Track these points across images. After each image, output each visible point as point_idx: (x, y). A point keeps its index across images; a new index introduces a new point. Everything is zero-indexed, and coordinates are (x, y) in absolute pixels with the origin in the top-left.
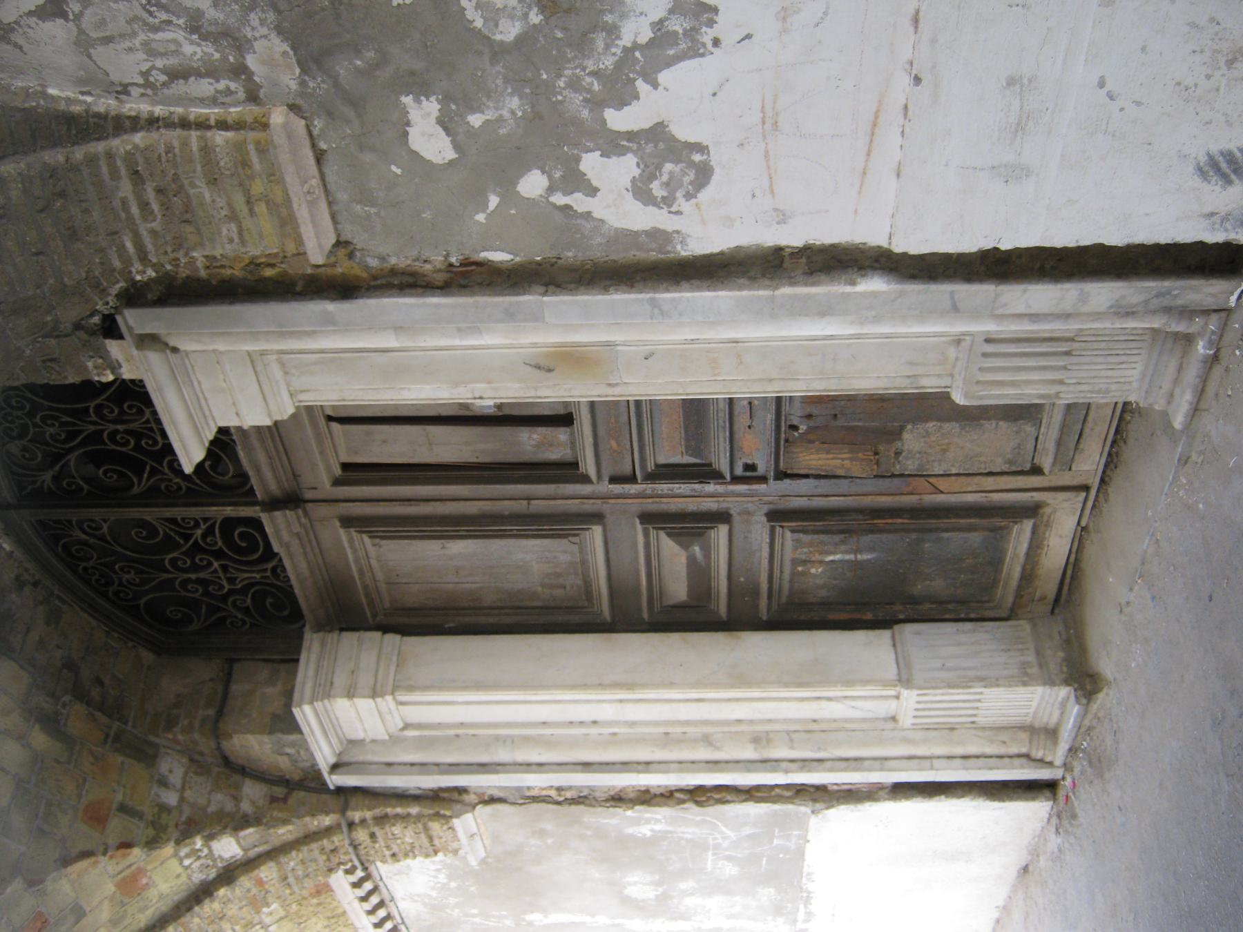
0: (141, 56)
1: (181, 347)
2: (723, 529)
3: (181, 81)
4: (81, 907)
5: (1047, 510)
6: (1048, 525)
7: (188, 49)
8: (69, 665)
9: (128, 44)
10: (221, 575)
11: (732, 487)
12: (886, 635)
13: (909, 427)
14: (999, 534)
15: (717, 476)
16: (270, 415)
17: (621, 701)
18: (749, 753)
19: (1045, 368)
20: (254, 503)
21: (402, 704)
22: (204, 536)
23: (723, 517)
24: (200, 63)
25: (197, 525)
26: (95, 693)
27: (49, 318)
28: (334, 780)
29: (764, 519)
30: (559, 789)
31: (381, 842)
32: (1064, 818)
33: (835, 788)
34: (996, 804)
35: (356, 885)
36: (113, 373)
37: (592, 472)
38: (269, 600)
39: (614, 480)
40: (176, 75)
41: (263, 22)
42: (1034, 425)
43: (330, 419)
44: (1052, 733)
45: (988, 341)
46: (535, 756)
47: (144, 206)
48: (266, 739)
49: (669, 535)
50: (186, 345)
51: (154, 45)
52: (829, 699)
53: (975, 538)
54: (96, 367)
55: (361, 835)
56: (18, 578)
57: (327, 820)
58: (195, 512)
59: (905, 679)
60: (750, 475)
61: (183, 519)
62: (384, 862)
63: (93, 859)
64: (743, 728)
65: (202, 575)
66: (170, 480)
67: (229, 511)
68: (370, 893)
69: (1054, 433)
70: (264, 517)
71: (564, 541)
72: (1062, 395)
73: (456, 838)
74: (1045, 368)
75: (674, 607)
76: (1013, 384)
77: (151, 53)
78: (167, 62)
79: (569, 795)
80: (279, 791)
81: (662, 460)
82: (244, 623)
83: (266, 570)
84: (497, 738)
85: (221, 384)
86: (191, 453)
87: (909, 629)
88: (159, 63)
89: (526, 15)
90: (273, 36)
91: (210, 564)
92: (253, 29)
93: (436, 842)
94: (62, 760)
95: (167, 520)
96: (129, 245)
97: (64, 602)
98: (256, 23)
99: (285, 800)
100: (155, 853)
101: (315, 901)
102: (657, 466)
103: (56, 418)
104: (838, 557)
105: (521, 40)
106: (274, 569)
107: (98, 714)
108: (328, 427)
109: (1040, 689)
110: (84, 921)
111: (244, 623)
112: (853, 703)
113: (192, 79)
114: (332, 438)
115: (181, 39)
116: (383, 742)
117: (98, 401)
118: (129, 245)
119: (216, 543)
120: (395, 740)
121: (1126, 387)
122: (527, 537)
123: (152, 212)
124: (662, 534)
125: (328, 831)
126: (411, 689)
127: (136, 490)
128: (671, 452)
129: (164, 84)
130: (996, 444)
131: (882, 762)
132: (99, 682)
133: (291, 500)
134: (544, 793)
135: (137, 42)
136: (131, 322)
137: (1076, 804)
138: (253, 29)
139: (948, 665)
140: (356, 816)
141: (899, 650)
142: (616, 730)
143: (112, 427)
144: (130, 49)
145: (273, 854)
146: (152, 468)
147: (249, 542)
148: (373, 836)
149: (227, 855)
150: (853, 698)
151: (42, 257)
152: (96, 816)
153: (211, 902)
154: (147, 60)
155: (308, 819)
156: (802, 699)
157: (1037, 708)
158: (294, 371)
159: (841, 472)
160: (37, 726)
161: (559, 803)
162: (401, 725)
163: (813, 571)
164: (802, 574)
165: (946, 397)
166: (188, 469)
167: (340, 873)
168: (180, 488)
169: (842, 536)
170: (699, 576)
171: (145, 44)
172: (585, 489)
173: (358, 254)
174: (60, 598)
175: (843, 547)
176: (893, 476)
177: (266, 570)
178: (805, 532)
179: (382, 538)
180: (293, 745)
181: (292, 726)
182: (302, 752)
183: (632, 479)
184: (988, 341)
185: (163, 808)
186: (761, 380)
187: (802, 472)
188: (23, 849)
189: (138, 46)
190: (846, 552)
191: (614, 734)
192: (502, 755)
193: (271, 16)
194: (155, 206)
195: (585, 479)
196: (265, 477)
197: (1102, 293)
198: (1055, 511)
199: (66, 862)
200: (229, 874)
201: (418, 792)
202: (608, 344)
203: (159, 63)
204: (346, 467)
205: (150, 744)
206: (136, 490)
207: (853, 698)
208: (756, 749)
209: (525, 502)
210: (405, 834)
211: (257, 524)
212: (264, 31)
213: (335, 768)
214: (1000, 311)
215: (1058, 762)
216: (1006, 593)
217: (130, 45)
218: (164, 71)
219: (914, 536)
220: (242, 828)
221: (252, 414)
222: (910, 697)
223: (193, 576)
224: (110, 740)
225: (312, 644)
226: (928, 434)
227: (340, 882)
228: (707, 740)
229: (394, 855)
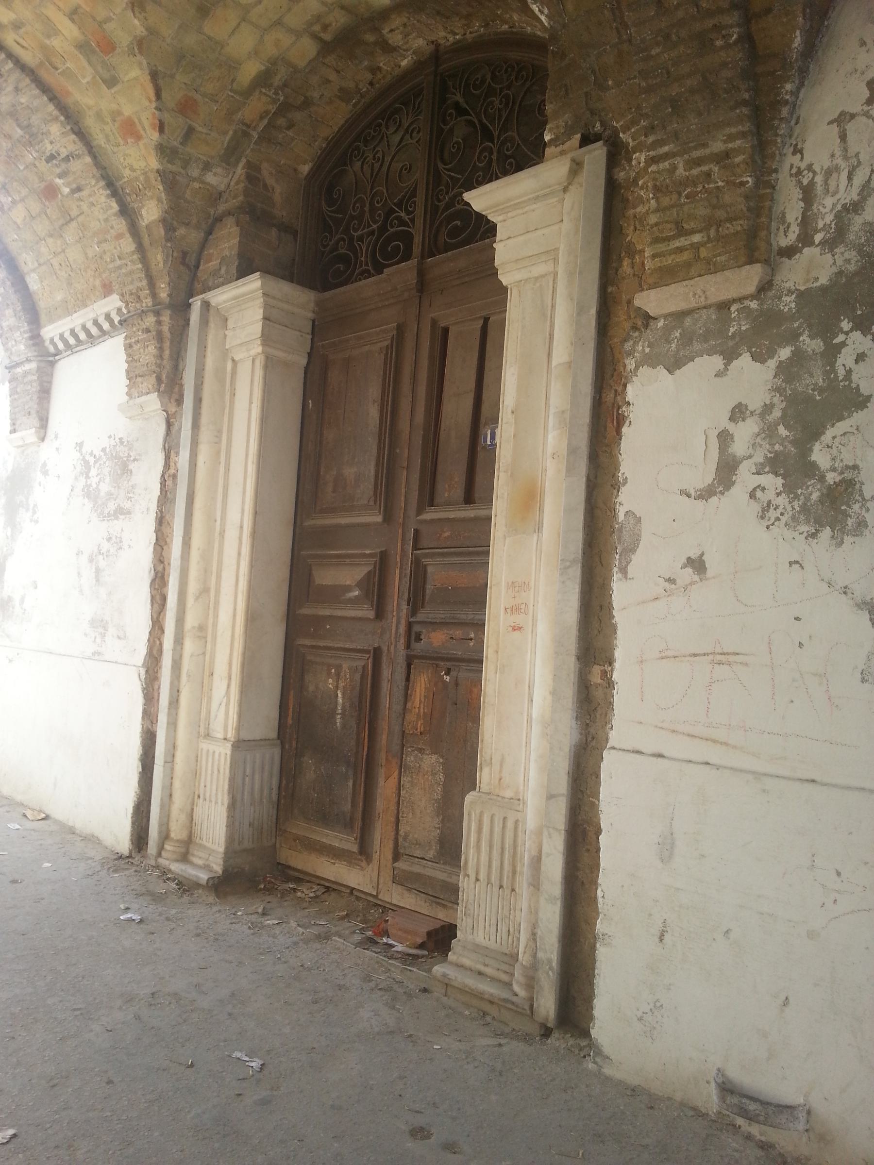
0: (827, 164)
1: (567, 196)
2: (371, 614)
3: (801, 196)
4: (115, 85)
5: (364, 864)
6: (350, 863)
7: (829, 201)
8: (307, 103)
9: (838, 153)
10: (366, 230)
11: (403, 622)
12: (274, 735)
13: (441, 760)
14: (348, 825)
15: (414, 612)
16: (503, 264)
17: (241, 527)
18: (191, 621)
19: (490, 866)
20: (423, 257)
21: (254, 360)
22: (399, 218)
23: (380, 614)
24: (815, 211)
25: (408, 213)
26: (281, 121)
27: (610, 83)
28: (196, 303)
29: (376, 645)
30: (174, 477)
31: (142, 336)
32: (118, 861)
33: (156, 687)
34: (130, 811)
35: (108, 317)
36: (551, 141)
37: (427, 516)
38: (342, 267)
39: (416, 532)
40: (808, 194)
41: (848, 261)
42: (434, 857)
43: (486, 320)
44: (184, 858)
45: (517, 822)
46: (201, 459)
47: (698, 162)
48: (235, 252)
49: (369, 572)
50: (569, 199)
51: (835, 175)
52: (229, 686)
53: (347, 807)
54: (558, 127)
55: (150, 320)
56: (379, 69)
57: (163, 295)
58: (419, 212)
59: (239, 745)
60: (412, 636)
61: (415, 202)
62: (126, 338)
63: (154, 99)
64: (211, 620)
65: (367, 215)
66: (447, 193)
67: (417, 240)
68: (100, 327)
69: (429, 872)
70: (413, 262)
71: (372, 493)
72: (466, 878)
73: (141, 394)
74: (490, 866)
75: (310, 574)
76: (479, 840)
77: (828, 173)
78: (819, 185)
79: (169, 483)
80: (192, 260)
81: (430, 569)
82: (325, 246)
83: (367, 265)
84: (220, 431)
85: (536, 223)
86: (480, 199)
87: (277, 752)
88: (819, 179)
89: (833, 469)
90: (835, 269)
91: (375, 222)
92: (842, 253)
93: (139, 379)
94: (234, 85)
95: (415, 189)
96: (666, 149)
97: (355, 105)
98: (847, 255)
99: (183, 263)
100: (153, 153)
101: (98, 283)
102: (426, 565)
103: (507, 104)
104: (340, 700)
105: (814, 465)
106: (368, 271)
107: (265, 121)
108: (481, 317)
109: (221, 849)
110: (104, 87)
111: (325, 246)
112: (224, 704)
113: (802, 204)
114: (470, 320)
115: (837, 197)
116: (224, 344)
117: (517, 138)
118: (666, 149)
119: (392, 227)
120: (225, 353)
121: (469, 930)
122: (377, 465)
123: (691, 169)
124: (371, 568)
125: (154, 295)
126: (266, 367)
127: (441, 166)
128: (438, 574)
129: (800, 182)
130: (421, 823)
131: (173, 724)
132: (290, 126)
133: (422, 286)
134: (172, 464)
135: (839, 161)
136: (597, 153)
137: (127, 872)
138: (842, 253)
139: (247, 779)
140: (166, 318)
141: (262, 743)
142: (218, 522)
143: (495, 150)
144: (833, 156)
145: (140, 248)
146: (459, 179)
147: (391, 249)
148: (148, 331)
149: (144, 212)
150: (228, 704)
151: (666, 76)
152: (186, 107)
153: (108, 196)
154: (822, 169)
155: (167, 279)
156: (230, 664)
157: (205, 847)
158: (538, 285)
159: (409, 705)
160: (263, 68)
161: (163, 476)
162: (236, 358)
163: (330, 681)
164: (329, 674)
165: (473, 787)
166: (468, 196)
167: (120, 304)
168: (440, 201)
169: (357, 704)
170: (334, 594)
171: (837, 169)
172: (412, 512)
173: (637, 334)
174: (359, 102)
175: (348, 704)
176: (403, 746)
177: (367, 265)
178: (363, 677)
179: (386, 355)
180: (227, 272)
181: (243, 272)
182: (221, 280)
183: (415, 548)
184: (517, 822)
185: (186, 164)
186: (498, 644)
187: (412, 676)
188: (169, 40)
189: (834, 162)
190: (343, 707)
191: (216, 521)
192: (205, 435)
193: (852, 268)
194: (695, 172)
195: (419, 512)
196: (445, 264)
197: (551, 916)
198: (362, 869)
199: (154, 76)
200: (126, 212)
201: (181, 367)
202: (539, 528)
203: (819, 179)
204: (446, 331)
205: (238, 161)
206: (441, 166)
207: (228, 704)
208: (194, 627)
209: (405, 465)
210: (148, 354)
211: (407, 257)
212: (840, 262)
213: (206, 305)
214: (545, 833)
215: (160, 860)
216: (299, 828)
217: (837, 156)
218: (812, 183)
219: (352, 760)
220: (165, 226)
221: (505, 251)
222: (225, 750)
223: (367, 209)
224: (244, 128)
225: (301, 300)
226: (434, 774)
227: (112, 304)
228: (205, 590)
229: (130, 346)
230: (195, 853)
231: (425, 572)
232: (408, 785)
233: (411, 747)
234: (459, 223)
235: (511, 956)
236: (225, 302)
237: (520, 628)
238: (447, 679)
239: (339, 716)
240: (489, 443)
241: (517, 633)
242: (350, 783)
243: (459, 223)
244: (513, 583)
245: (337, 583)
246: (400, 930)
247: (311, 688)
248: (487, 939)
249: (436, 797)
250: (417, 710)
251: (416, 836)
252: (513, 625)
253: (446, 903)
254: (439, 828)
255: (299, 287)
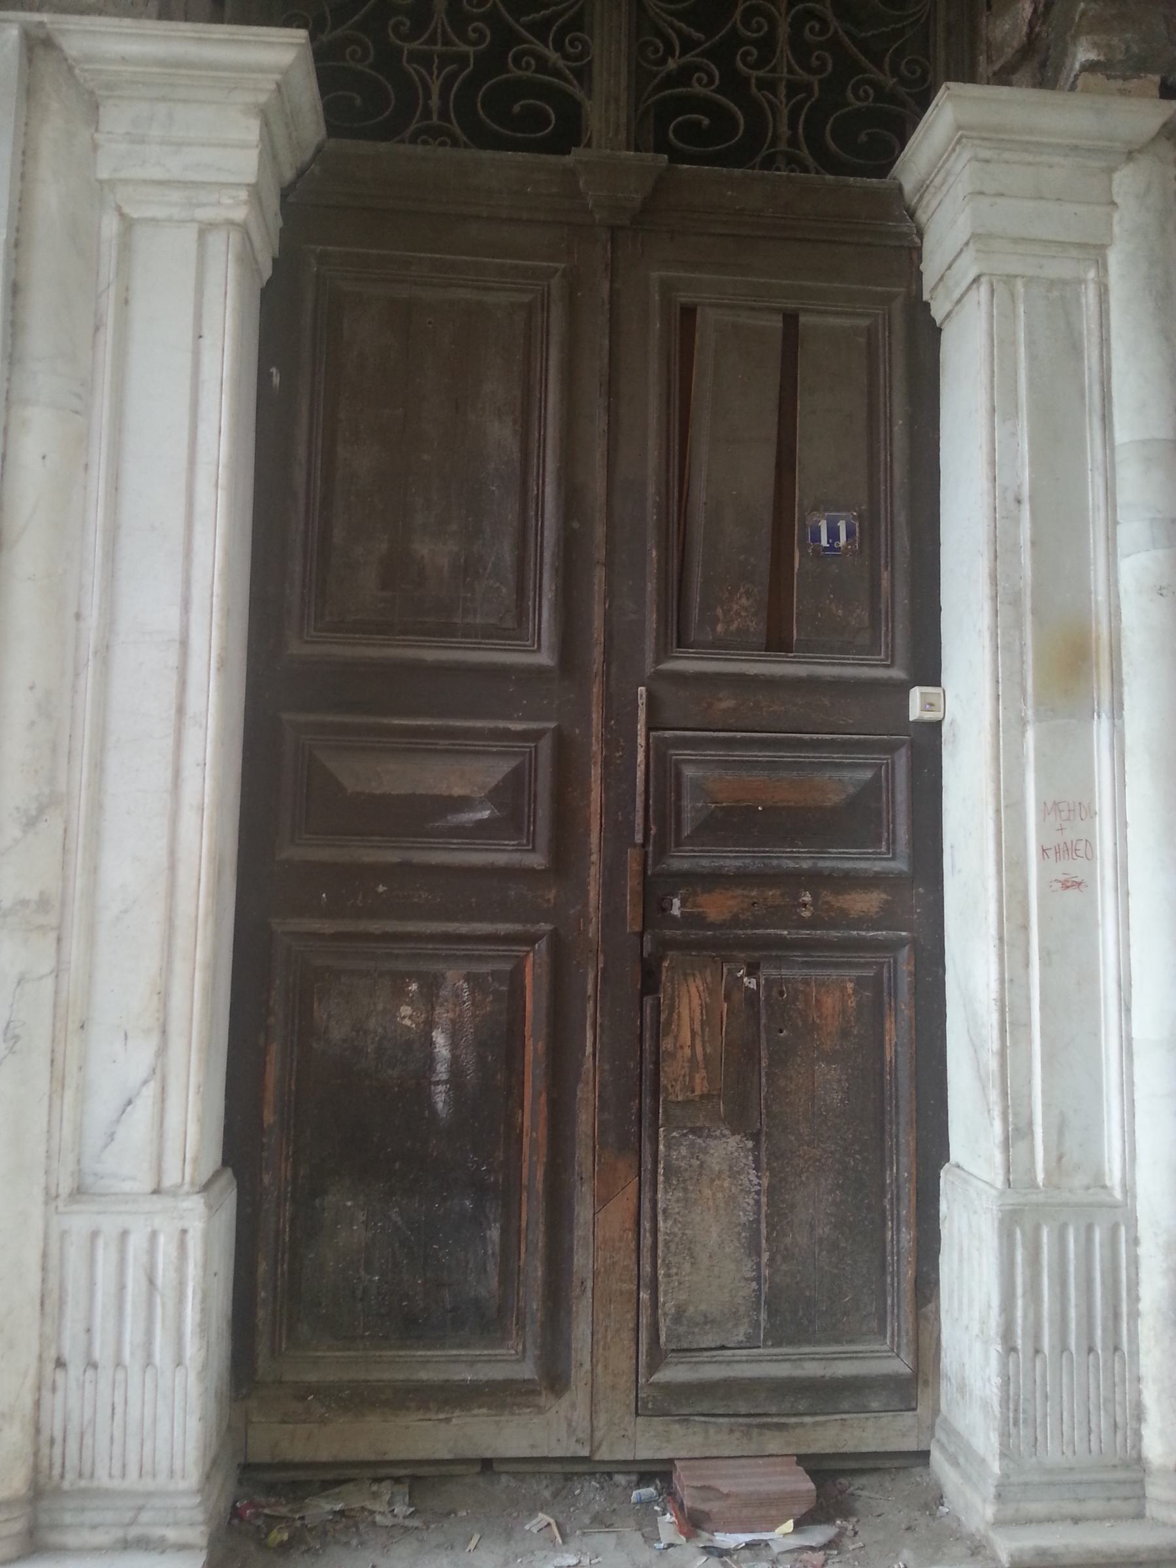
17: (184, 643)
49: (516, 773)
64: (79, 883)
156: (164, 995)
157: (107, 1493)
204: (689, 313)
226: (734, 1175)
230: (68, 1518)
231: (679, 775)
232: (675, 1208)
233: (678, 1128)
234: (706, 122)
235: (1126, 1466)
236: (124, 60)
237: (1079, 884)
238: (750, 983)
239: (441, 1088)
240: (824, 542)
241: (1072, 893)
242: (494, 1233)
243: (706, 122)
244: (1056, 804)
245: (420, 791)
246: (746, 1505)
247: (338, 1033)
248: (1069, 1453)
249: (743, 1219)
250: (688, 1051)
251: (703, 1307)
252: (1062, 878)
253: (784, 1420)
254: (752, 1280)
255: (320, 108)
